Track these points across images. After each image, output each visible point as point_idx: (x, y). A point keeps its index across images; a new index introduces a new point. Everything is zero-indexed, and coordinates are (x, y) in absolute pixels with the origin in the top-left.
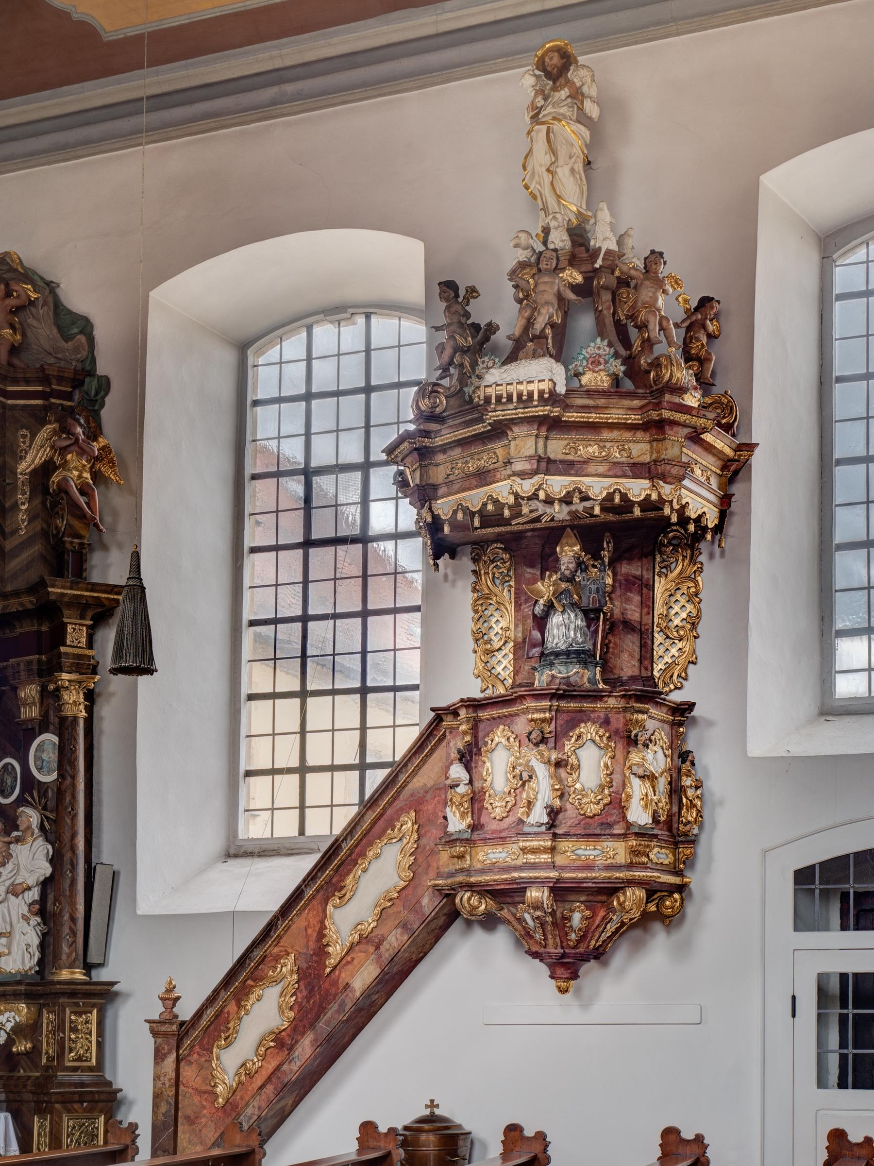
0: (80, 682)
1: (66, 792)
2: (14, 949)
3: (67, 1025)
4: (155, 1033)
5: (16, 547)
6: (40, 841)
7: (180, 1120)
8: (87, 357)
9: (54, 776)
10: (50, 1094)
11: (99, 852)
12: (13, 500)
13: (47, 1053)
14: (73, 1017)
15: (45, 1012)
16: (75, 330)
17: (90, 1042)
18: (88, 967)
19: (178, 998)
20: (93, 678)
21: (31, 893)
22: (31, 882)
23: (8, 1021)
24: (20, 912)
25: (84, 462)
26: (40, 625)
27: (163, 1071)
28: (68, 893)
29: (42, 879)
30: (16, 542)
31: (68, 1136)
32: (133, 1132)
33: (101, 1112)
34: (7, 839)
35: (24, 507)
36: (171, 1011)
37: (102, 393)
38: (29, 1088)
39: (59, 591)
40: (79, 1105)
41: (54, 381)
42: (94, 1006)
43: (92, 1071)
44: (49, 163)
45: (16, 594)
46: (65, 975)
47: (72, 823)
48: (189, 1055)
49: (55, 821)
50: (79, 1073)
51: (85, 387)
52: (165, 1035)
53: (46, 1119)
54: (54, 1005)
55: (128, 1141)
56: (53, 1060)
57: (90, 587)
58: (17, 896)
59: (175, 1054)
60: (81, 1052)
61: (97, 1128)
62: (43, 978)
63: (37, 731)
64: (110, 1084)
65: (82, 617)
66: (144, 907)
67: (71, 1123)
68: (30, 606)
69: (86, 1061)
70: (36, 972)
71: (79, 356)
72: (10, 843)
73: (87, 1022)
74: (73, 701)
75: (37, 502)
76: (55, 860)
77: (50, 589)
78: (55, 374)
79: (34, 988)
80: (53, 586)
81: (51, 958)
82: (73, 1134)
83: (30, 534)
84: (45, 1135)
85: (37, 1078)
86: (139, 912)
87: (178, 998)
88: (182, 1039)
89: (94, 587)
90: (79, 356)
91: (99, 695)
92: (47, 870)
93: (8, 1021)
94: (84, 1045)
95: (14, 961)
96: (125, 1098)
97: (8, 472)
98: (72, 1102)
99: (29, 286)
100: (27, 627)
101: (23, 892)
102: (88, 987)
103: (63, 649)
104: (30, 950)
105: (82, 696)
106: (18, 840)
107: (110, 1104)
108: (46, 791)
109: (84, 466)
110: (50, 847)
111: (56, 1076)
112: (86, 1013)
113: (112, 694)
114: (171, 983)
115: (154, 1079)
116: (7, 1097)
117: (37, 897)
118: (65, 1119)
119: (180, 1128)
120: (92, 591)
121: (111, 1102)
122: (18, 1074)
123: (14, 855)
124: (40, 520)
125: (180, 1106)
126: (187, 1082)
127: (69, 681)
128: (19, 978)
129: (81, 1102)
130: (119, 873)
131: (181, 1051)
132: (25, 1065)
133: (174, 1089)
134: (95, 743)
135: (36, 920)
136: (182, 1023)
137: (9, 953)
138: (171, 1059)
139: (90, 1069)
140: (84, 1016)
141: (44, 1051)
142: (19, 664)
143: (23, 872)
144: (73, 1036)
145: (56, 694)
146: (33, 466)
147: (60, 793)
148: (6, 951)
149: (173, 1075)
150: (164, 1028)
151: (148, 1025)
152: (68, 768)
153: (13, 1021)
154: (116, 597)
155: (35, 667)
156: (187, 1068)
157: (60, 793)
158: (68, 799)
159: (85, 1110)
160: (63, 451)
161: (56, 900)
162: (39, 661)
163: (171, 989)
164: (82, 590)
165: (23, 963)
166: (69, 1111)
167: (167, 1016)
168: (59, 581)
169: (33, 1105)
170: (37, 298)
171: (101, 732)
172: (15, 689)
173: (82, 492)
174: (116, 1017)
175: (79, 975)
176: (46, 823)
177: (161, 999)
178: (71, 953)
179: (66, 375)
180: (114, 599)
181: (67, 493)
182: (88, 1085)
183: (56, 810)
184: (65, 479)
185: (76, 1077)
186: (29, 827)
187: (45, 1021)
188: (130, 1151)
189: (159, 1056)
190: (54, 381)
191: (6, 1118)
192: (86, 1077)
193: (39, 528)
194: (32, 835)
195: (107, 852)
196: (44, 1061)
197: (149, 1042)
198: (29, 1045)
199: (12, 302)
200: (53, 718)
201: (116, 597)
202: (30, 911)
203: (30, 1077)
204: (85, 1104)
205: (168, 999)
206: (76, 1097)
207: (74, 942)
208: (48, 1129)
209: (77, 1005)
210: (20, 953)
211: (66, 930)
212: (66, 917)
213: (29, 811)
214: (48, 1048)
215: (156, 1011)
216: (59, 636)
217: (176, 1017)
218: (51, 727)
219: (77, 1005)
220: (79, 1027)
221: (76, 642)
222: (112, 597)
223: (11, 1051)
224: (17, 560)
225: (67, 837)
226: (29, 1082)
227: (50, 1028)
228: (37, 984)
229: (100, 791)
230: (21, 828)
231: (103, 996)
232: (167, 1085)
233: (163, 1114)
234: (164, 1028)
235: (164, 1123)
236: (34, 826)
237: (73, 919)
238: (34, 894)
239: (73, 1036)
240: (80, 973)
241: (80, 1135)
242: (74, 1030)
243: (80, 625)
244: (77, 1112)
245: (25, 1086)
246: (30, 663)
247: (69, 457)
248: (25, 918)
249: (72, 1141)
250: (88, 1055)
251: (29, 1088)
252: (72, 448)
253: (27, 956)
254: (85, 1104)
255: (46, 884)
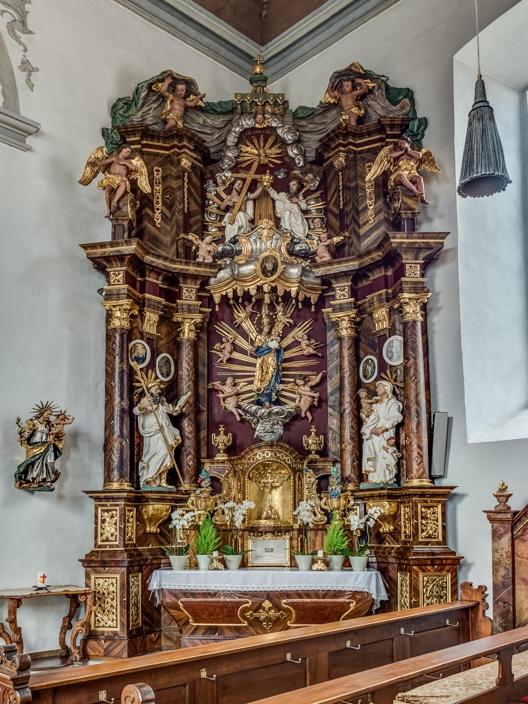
0: (417, 299)
1: (410, 368)
2: (378, 468)
3: (419, 514)
4: (491, 520)
5: (368, 231)
6: (394, 400)
7: (517, 581)
8: (410, 110)
9: (401, 360)
10: (409, 560)
11: (436, 406)
12: (364, 205)
13: (405, 532)
14: (423, 510)
15: (402, 507)
16: (401, 97)
17: (437, 526)
18: (432, 478)
19: (510, 495)
20: (427, 295)
21: (388, 433)
22: (388, 425)
23: (375, 512)
24: (381, 445)
25: (412, 164)
26: (386, 271)
27: (500, 546)
28: (415, 431)
29: (396, 423)
30: (367, 229)
31: (424, 587)
32: (483, 593)
33: (448, 571)
34: (370, 401)
35: (371, 208)
36: (505, 505)
37: (422, 127)
38: (393, 554)
39: (399, 240)
40: (431, 567)
41: (388, 129)
42: (439, 502)
43: (439, 545)
44: (377, 14)
45: (369, 253)
46: (416, 482)
47: (416, 387)
48: (522, 535)
49: (403, 388)
50: (430, 546)
51: (410, 128)
52: (501, 521)
53: (406, 576)
54: (409, 502)
55: (479, 599)
56: (410, 537)
57: (421, 235)
58: (378, 435)
59: (510, 535)
60: (431, 532)
61: (446, 583)
62: (399, 485)
63: (388, 336)
64: (454, 553)
65: (416, 258)
66: (472, 439)
67: (425, 579)
68: (378, 259)
69: (435, 538)
70: (394, 482)
71: (404, 111)
72: (372, 404)
73: (434, 513)
74: (412, 311)
75: (380, 203)
76: (405, 411)
77: (392, 240)
78: (389, 123)
79: (393, 492)
80: (394, 238)
81: (405, 473)
82: (428, 586)
83: (376, 222)
84: (406, 586)
85: (398, 548)
86: (469, 442)
87: (510, 495)
88: (516, 524)
89: (424, 235)
90: (404, 111)
91: (431, 310)
92: (400, 418)
93: (375, 512)
94: (432, 527)
95: (379, 476)
96: (465, 562)
97: (359, 190)
98: (425, 565)
99: (368, 80)
100: (378, 274)
101: (383, 432)
102: (433, 490)
103: (403, 279)
104: (390, 468)
105: (418, 308)
106: (377, 402)
107: (455, 567)
108: (396, 372)
109: (412, 166)
110: (400, 404)
111: (413, 548)
112: (433, 507)
113: (441, 308)
114: (503, 484)
115: (493, 552)
116: (377, 560)
117: (393, 435)
118: (421, 575)
119: (517, 587)
120: (423, 238)
121: (456, 565)
122: (385, 546)
123: (375, 410)
124: (383, 213)
125: (516, 571)
126: (522, 554)
127: (409, 299)
128: (382, 486)
129: (433, 565)
130: (452, 418)
131: (515, 532)
132: (389, 540)
133: (511, 559)
134: (429, 340)
135: (392, 449)
136: (515, 513)
137: (375, 471)
138: (507, 538)
139: (438, 543)
140: (431, 509)
141: (403, 532)
142: (373, 298)
143: (382, 421)
144: (424, 522)
145: (400, 310)
146: (376, 175)
147: (406, 370)
148: (372, 470)
149: (510, 549)
150: (499, 516)
151: (486, 514)
152: (411, 353)
153: (379, 513)
154: (441, 241)
155: (384, 297)
156: (521, 544)
157: (406, 370)
158: (412, 372)
159: (435, 571)
160: (397, 159)
161: (406, 436)
162: (387, 293)
163: (503, 489)
164: (415, 239)
165: (385, 476)
166: (423, 571)
167: (501, 508)
168: (399, 234)
169: (396, 565)
170: (374, 87)
171: (434, 333)
172: (371, 315)
173: (414, 182)
174: (455, 509)
175: (426, 482)
176: (397, 390)
177: (496, 496)
178: (420, 469)
179: (396, 123)
180: (439, 242)
181: (401, 184)
182: (437, 554)
183: (404, 381)
184: (400, 176)
185: (427, 549)
186: (385, 393)
187: (402, 513)
188: (481, 607)
189: (496, 536)
190: (388, 129)
191: (377, 575)
192: (436, 549)
193: (383, 217)
194: (387, 397)
195: (443, 404)
196: (403, 538)
197: (488, 527)
198: (392, 528)
199: (359, 92)
200: (399, 327)
201: (441, 241)
202: (388, 444)
203: (393, 548)
204: (436, 567)
205: (502, 496)
206: (429, 562)
207: (422, 461)
208: (408, 582)
209: (426, 502)
210: (382, 470)
211: (415, 454)
212: (415, 446)
213: (384, 383)
214: (406, 529)
215: (492, 504)
216: (400, 272)
217: (509, 508)
218: (398, 332)
219: (426, 502)
220: (428, 516)
221: (412, 275)
222: (438, 241)
223: (379, 532)
224: (369, 239)
225: (412, 396)
226: (393, 551)
227: (407, 517)
228: (396, 489)
229: (434, 369)
230: (379, 394)
231: (446, 496)
232: (505, 556)
233: (502, 577)
234: (499, 516)
235: (503, 583)
236: (388, 392)
237: (420, 447)
238: (391, 433)
239: (424, 522)
240: (427, 481)
241: (433, 587)
242: (424, 518)
243: (415, 264)
244: (430, 571)
245: (390, 553)
246: (381, 295)
247: (401, 163)
248: (386, 449)
249: (427, 590)
250: (436, 534)
251: (393, 554)
252: (403, 157)
253: (387, 472)
254: (436, 567)
255: (399, 426)
